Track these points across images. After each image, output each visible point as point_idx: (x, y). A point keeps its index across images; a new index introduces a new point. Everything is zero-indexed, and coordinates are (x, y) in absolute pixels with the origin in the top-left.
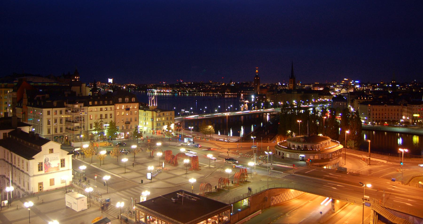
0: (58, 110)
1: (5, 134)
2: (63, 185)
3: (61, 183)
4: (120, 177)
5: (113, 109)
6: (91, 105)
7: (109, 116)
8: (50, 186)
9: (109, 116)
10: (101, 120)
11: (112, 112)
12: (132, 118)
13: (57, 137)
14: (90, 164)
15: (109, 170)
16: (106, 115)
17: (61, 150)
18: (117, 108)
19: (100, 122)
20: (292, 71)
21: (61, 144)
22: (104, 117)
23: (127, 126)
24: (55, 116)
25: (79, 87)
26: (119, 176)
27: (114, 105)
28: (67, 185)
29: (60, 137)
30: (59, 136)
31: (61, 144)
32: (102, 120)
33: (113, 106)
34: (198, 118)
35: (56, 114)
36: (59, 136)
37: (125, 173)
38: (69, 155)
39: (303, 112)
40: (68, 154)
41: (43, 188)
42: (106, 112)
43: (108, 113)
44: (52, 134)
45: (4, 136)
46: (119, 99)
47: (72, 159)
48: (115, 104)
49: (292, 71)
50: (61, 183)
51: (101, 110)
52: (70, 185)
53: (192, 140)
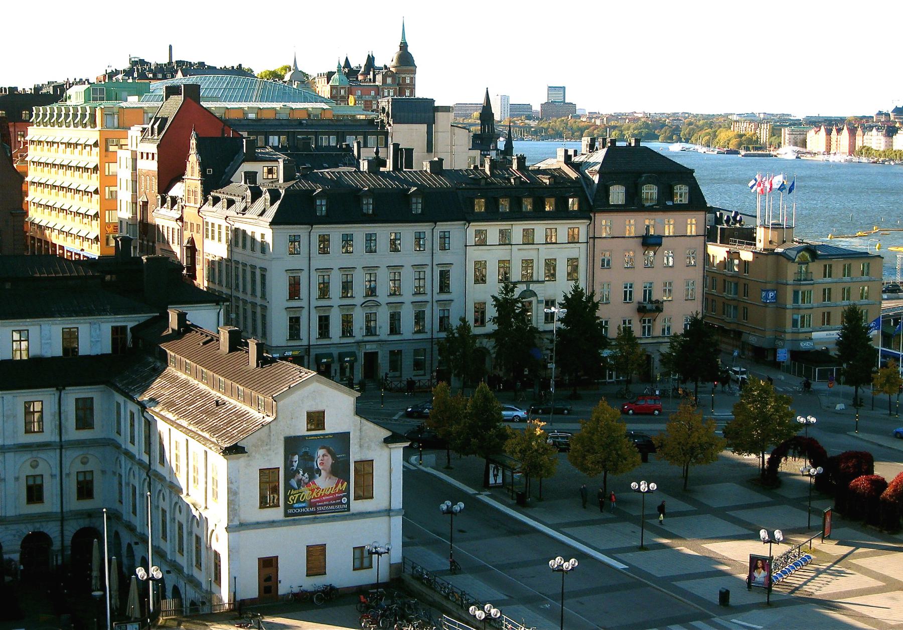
0: (336, 232)
1: (118, 332)
2: (366, 577)
3: (354, 569)
4: (620, 566)
5: (583, 238)
6: (480, 213)
7: (562, 269)
8: (307, 576)
9: (562, 269)
10: (528, 287)
11: (579, 251)
12: (670, 284)
13: (330, 355)
14: (479, 494)
15: (566, 530)
16: (551, 266)
17: (358, 418)
18: (601, 233)
19: (523, 295)
20: (403, 30)
21: (359, 394)
22: (540, 272)
23: (649, 321)
24: (320, 261)
25: (424, 127)
26: (615, 558)
27: (590, 219)
28: (379, 582)
29: (341, 356)
30: (336, 355)
31: (359, 394)
32: (532, 287)
33: (581, 227)
34: (689, 226)
35: (324, 251)
36: (336, 355)
37: (642, 548)
38: (391, 446)
39: (11, 560)
40: (387, 441)
41: (277, 582)
42: (529, 253)
43: (562, 256)
44: (305, 342)
45: (114, 341)
46: (687, 202)
47: (404, 466)
48: (592, 215)
49: (403, 30)
50: (354, 569)
51: (528, 239)
52: (392, 580)
53: (694, 461)
